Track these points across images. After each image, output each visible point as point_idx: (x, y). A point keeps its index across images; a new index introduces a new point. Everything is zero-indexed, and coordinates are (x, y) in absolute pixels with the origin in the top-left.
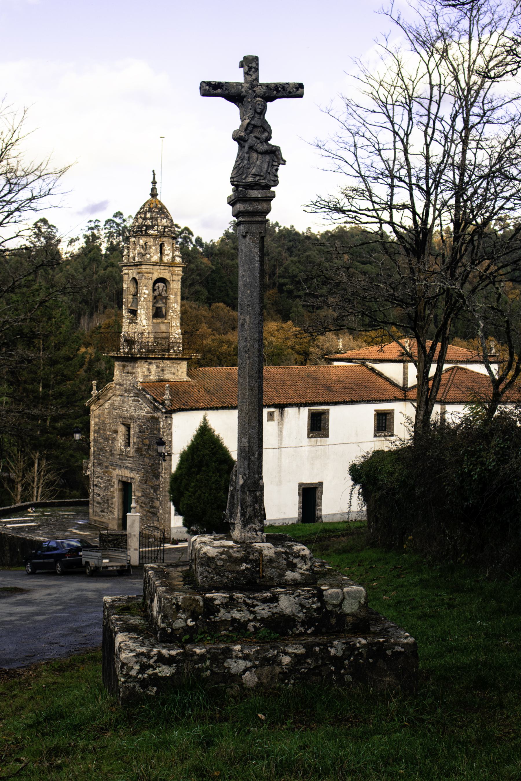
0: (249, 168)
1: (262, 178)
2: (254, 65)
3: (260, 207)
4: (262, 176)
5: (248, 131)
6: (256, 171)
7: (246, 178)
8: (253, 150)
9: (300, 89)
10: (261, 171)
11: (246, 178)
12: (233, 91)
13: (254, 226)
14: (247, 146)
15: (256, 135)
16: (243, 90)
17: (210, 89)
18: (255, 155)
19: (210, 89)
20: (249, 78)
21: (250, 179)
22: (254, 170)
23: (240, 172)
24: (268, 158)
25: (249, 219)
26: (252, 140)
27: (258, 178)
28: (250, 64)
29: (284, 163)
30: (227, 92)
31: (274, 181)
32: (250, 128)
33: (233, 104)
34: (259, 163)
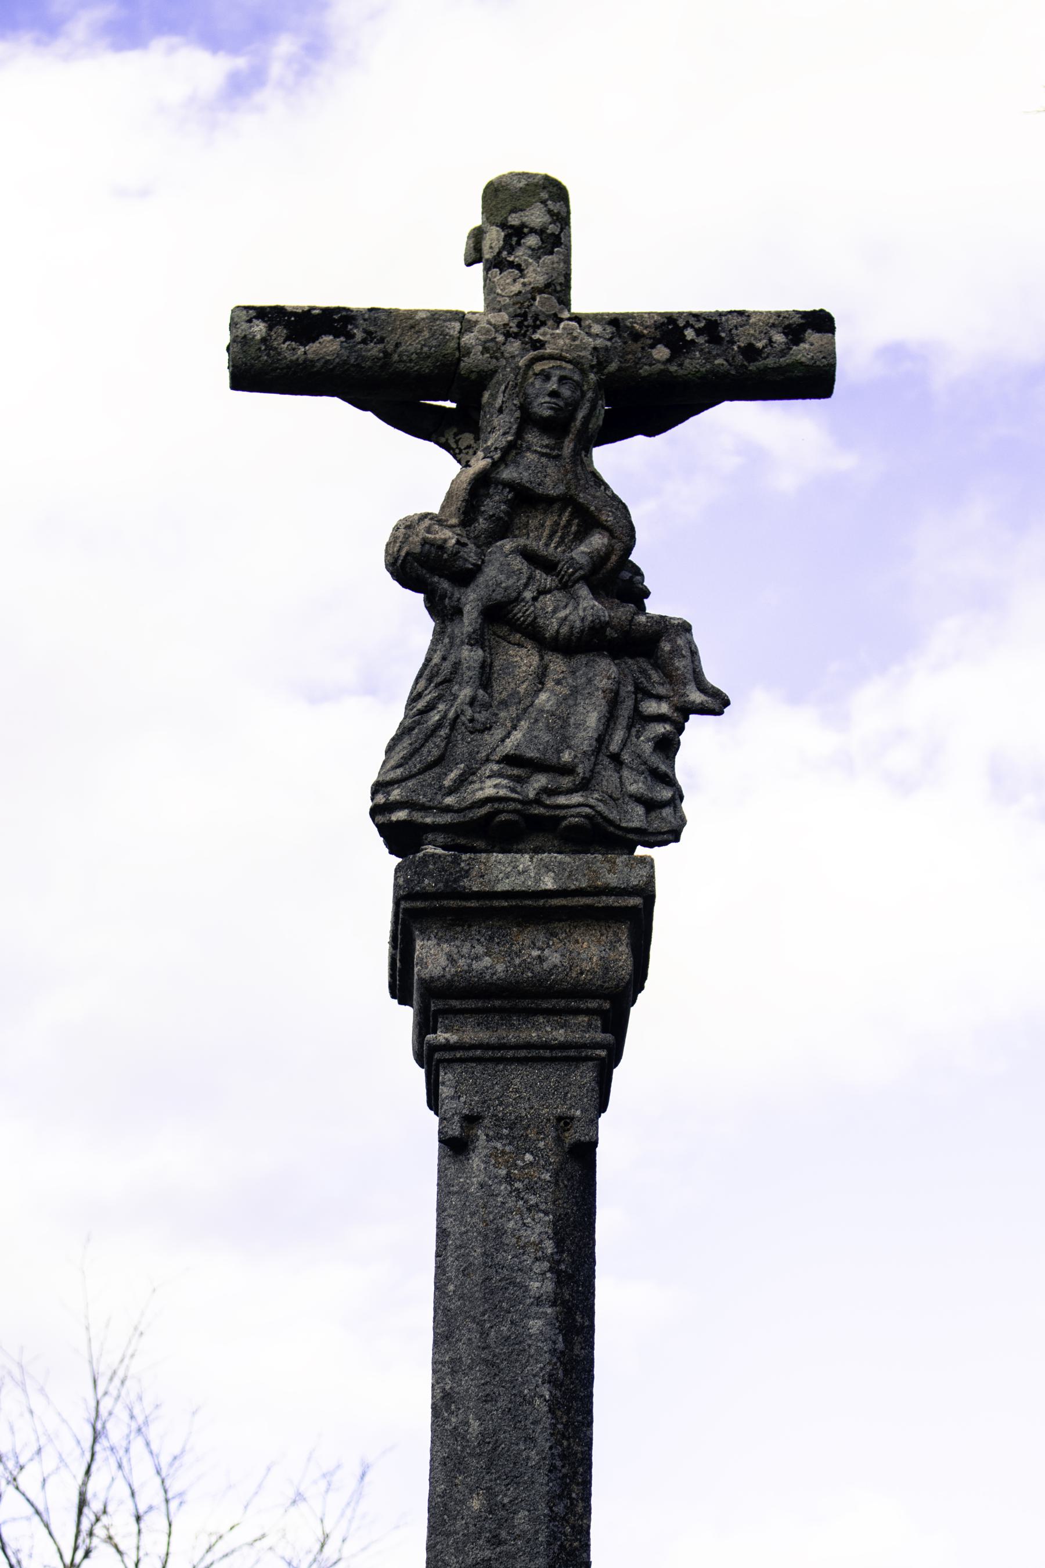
0: (487, 728)
1: (566, 782)
2: (536, 216)
3: (554, 958)
4: (567, 770)
5: (482, 524)
6: (531, 739)
7: (462, 781)
8: (516, 627)
9: (813, 338)
10: (565, 742)
11: (462, 781)
12: (411, 344)
13: (519, 1077)
14: (471, 601)
15: (537, 544)
16: (468, 339)
17: (285, 352)
18: (524, 659)
19: (285, 352)
20: (510, 285)
21: (489, 787)
22: (517, 736)
23: (432, 751)
24: (605, 671)
25: (483, 1036)
26: (502, 568)
27: (540, 781)
28: (525, 222)
29: (717, 703)
30: (374, 350)
31: (651, 805)
32: (494, 504)
33: (431, 447)
34: (560, 704)
